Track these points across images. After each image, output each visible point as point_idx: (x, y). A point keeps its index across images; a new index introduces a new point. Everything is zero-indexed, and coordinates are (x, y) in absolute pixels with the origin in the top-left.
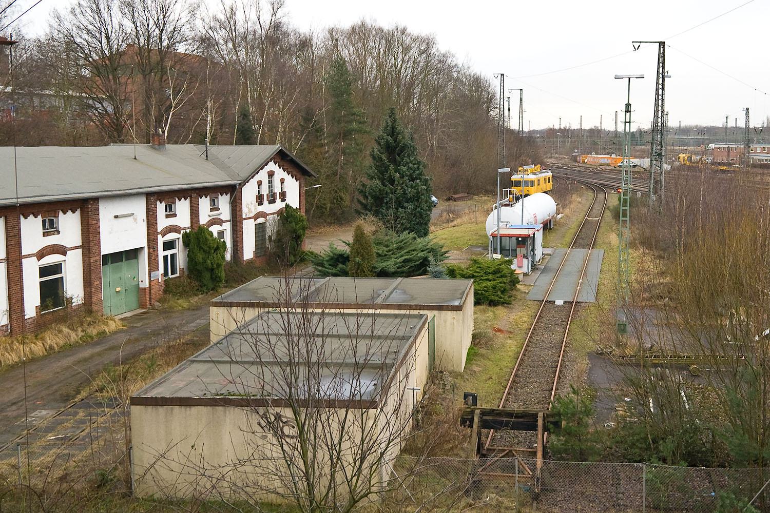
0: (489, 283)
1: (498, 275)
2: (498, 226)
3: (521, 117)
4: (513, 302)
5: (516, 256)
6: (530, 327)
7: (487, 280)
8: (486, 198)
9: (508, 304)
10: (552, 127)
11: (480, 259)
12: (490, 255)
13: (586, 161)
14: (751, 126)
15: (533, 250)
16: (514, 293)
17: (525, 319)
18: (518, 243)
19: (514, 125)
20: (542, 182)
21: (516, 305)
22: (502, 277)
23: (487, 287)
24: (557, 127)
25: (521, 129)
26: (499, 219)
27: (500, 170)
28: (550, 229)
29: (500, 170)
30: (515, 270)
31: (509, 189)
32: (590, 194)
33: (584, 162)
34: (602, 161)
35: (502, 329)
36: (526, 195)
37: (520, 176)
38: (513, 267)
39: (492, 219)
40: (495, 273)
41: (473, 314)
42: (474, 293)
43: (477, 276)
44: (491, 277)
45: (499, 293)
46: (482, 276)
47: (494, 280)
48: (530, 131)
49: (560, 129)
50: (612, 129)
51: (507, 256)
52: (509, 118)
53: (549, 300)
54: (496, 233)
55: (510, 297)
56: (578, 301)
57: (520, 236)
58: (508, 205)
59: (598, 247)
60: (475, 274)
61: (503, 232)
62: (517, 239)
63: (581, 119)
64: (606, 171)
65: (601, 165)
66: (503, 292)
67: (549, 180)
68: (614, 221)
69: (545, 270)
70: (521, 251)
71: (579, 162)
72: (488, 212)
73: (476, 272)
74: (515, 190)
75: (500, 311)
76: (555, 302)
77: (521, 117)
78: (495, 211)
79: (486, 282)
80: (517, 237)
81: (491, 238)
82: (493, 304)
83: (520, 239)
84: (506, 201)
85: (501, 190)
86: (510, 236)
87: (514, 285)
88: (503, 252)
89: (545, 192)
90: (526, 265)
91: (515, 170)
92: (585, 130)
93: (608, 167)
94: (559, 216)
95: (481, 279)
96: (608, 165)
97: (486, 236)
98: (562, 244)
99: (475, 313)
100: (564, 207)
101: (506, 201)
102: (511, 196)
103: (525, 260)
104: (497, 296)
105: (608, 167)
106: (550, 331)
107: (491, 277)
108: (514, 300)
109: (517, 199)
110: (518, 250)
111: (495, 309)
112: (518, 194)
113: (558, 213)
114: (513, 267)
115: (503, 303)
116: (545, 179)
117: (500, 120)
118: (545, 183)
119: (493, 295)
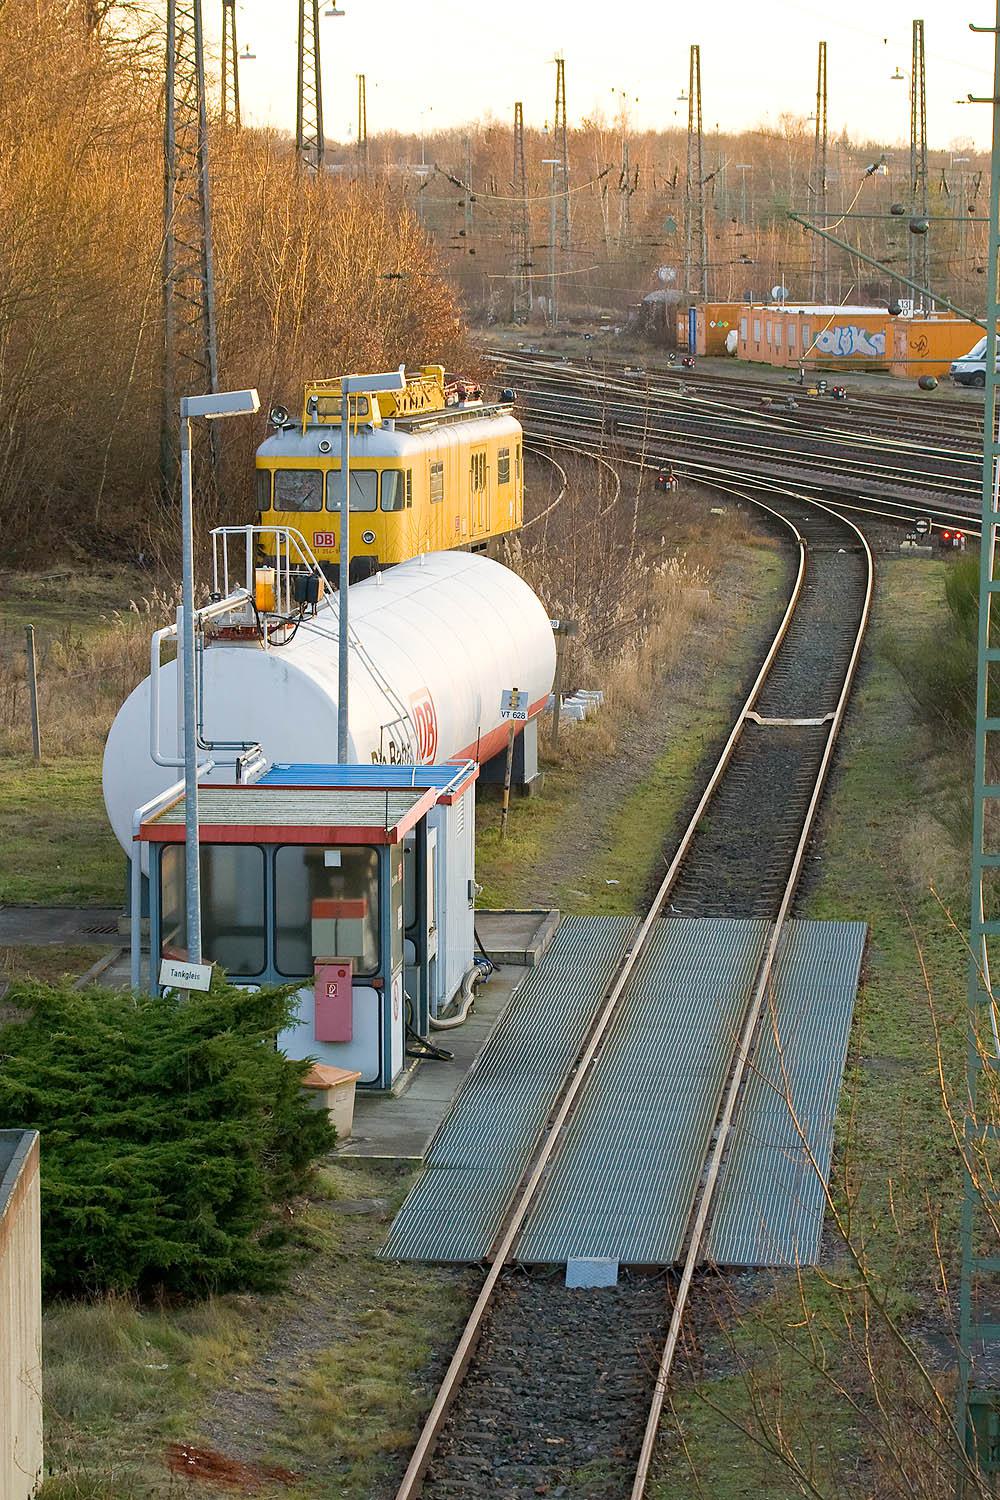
0: (138, 1156)
1: (194, 1101)
2: (188, 769)
3: (309, 51)
4: (300, 1279)
5: (307, 974)
6: (404, 1436)
7: (125, 1131)
8: (94, 585)
9: (265, 1289)
10: (507, 120)
11: (71, 988)
12: (134, 967)
13: (732, 340)
14: (933, 145)
15: (416, 931)
16: (309, 1216)
17: (373, 1388)
18: (320, 879)
19: (266, 104)
20: (460, 475)
21: (312, 1288)
22: (219, 1110)
23: (125, 1184)
24: (539, 119)
25: (309, 132)
26: (190, 723)
27: (199, 405)
28: (522, 790)
29: (199, 405)
30: (304, 1067)
31: (250, 530)
32: (764, 559)
33: (718, 350)
34: (831, 342)
35: (228, 1452)
36: (363, 569)
37: (314, 439)
38: (293, 1044)
39: (146, 716)
40: (172, 1085)
41: (36, 1360)
42: (44, 1224)
43: (59, 1112)
44: (145, 1112)
45: (206, 1218)
46: (89, 1109)
47: (172, 1133)
48: (364, 146)
49: (562, 132)
50: (895, 134)
51: (246, 972)
52: (233, 58)
53: (529, 1254)
54: (177, 819)
55: (275, 1241)
56: (714, 1258)
57: (333, 838)
58: (242, 635)
59: (829, 906)
60: (45, 1097)
61: (215, 811)
62: (315, 862)
63: (561, 76)
64: (864, 417)
65: (826, 366)
66: (226, 1213)
67: (504, 466)
68: (923, 734)
69: (498, 1063)
70: (344, 937)
71: (689, 349)
72: (115, 683)
73: (47, 1082)
74: (284, 531)
75: (219, 1339)
76: (562, 1269)
77: (309, 51)
78: (166, 678)
79: (115, 1144)
80: (312, 843)
81: (141, 857)
82: (167, 1288)
83: (333, 859)
84: (229, 606)
85: (203, 538)
86: (268, 842)
87: (298, 1163)
88: (223, 944)
89: (474, 550)
90: (376, 1026)
91: (283, 409)
92: (717, 139)
93: (870, 385)
94: (580, 704)
95: (84, 1131)
96: (876, 368)
97: (104, 836)
98: (593, 887)
99: (51, 1355)
100: (605, 644)
101: (229, 606)
102: (266, 576)
103: (366, 997)
104: (193, 1236)
105: (870, 385)
106: (537, 1460)
107: (145, 1112)
108: (304, 1261)
109: (305, 592)
110: (321, 928)
111: (607, 1285)
112: (311, 558)
113: (567, 683)
114: (293, 1044)
115: (230, 1284)
116: (478, 462)
117: (171, 60)
118: (479, 481)
119: (166, 1234)
